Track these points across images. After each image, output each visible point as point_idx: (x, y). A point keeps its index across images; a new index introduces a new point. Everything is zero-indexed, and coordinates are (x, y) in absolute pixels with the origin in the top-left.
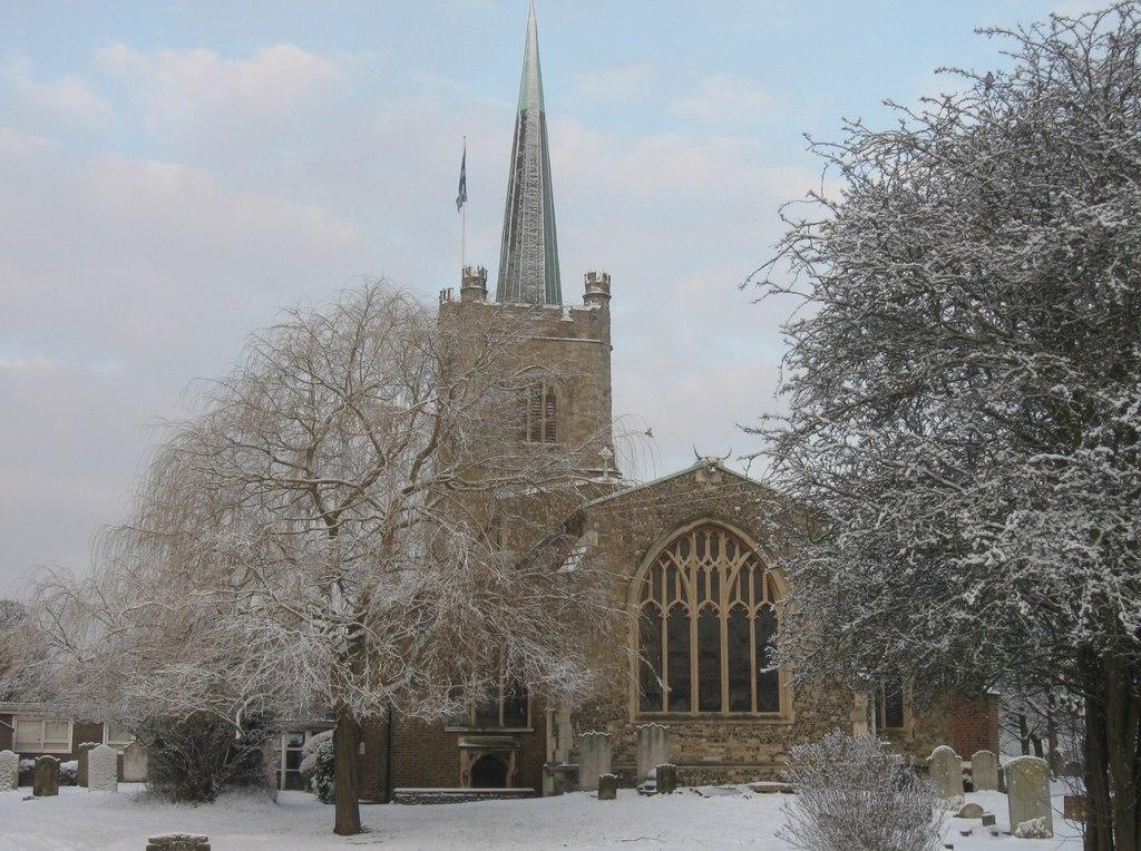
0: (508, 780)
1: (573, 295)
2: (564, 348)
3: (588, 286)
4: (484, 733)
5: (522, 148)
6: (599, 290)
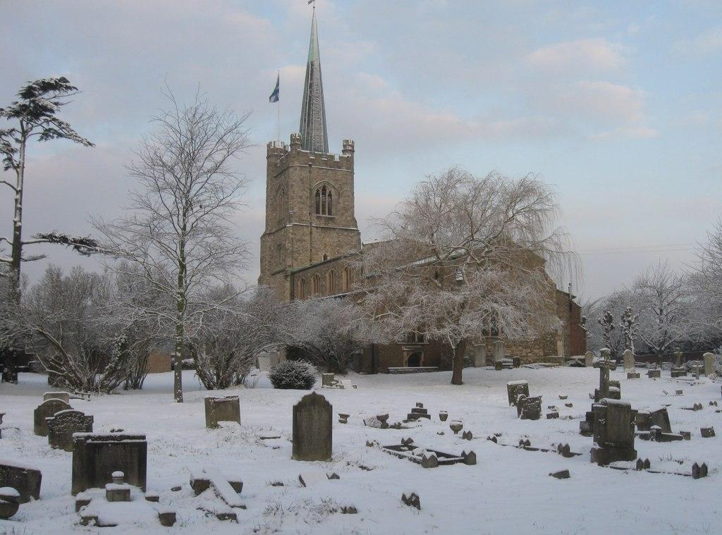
0: (421, 363)
1: (335, 150)
2: (335, 173)
3: (344, 146)
4: (412, 345)
5: (311, 79)
6: (350, 148)
